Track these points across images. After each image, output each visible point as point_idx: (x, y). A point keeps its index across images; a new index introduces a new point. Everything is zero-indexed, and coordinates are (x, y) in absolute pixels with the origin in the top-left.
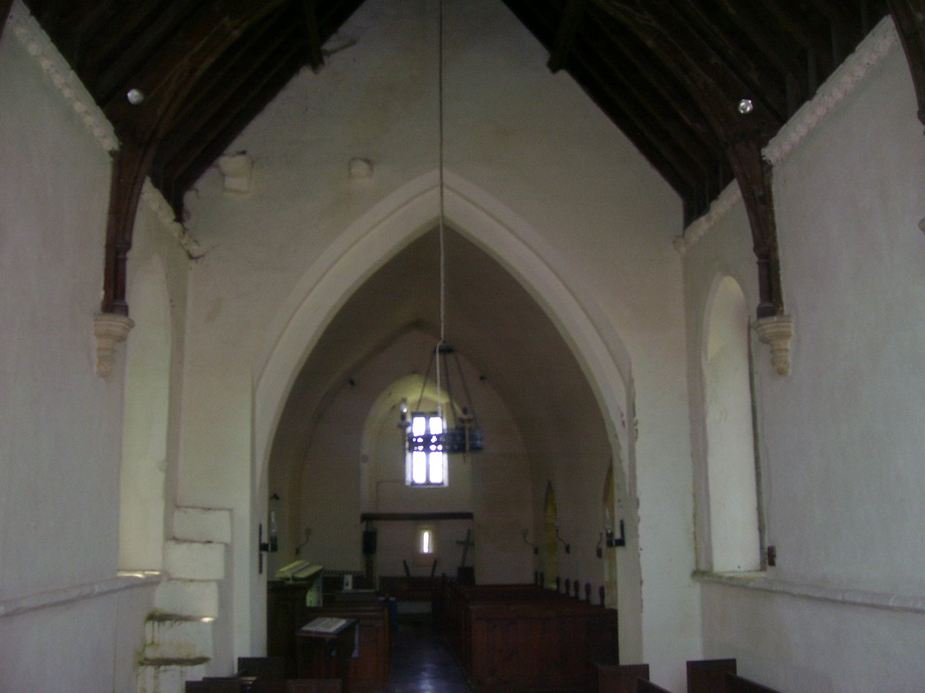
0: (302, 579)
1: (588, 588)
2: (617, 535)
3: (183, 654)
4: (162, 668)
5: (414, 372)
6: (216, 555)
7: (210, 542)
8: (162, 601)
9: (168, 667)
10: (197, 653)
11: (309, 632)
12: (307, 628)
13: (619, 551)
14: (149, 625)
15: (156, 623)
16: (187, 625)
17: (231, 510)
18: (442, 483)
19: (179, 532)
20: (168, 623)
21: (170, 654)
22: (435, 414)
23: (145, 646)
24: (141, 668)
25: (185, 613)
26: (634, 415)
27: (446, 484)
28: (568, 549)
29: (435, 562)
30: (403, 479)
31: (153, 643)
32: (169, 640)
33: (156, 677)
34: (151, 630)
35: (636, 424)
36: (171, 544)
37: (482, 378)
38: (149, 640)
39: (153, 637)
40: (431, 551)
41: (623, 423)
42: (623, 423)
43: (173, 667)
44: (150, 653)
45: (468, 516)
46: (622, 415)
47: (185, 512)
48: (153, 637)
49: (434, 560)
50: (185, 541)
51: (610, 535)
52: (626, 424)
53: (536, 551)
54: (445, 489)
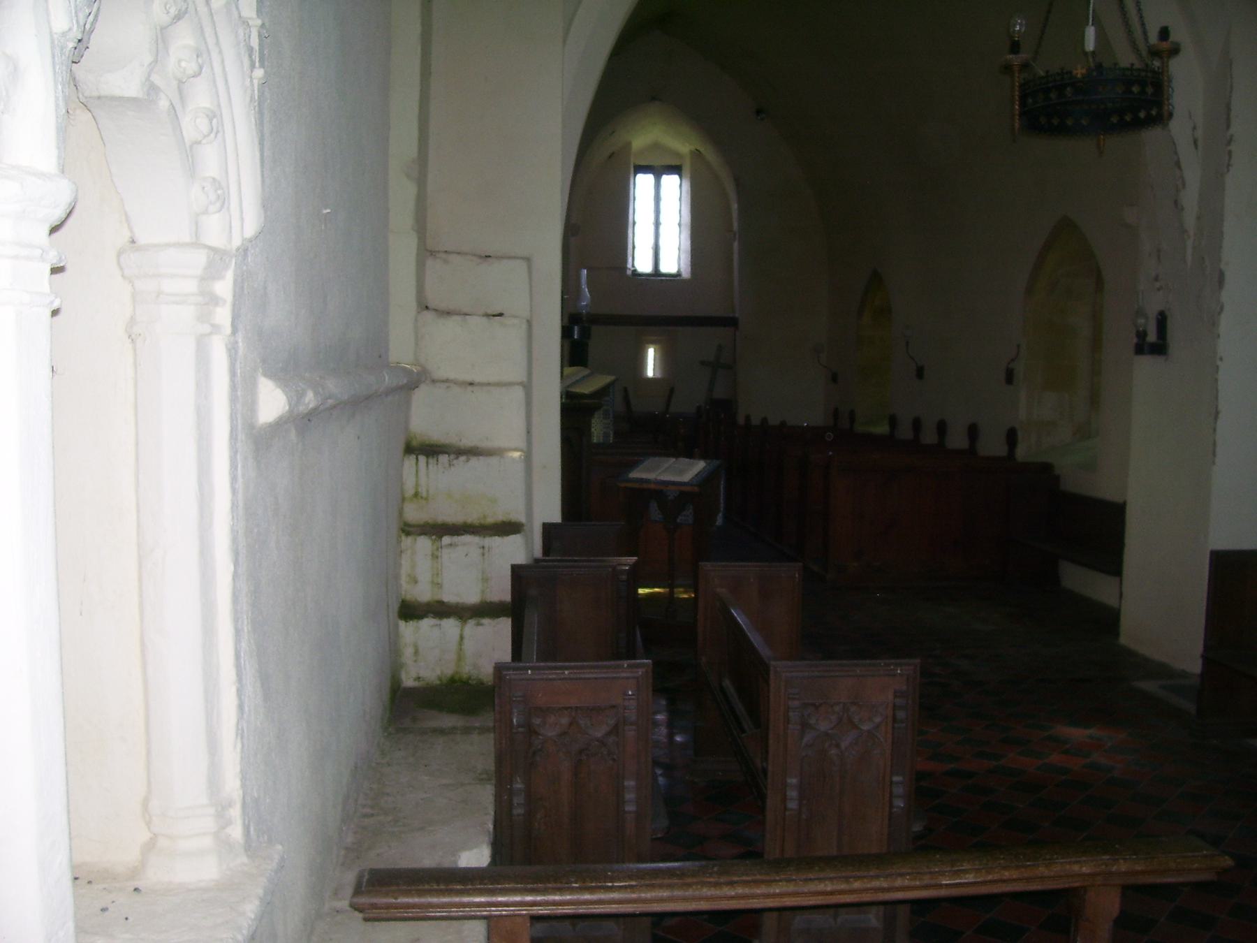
0: (583, 396)
1: (917, 425)
2: (1152, 337)
3: (473, 517)
4: (446, 540)
5: (653, 99)
6: (510, 337)
7: (501, 315)
8: (426, 418)
9: (456, 539)
10: (498, 514)
11: (642, 481)
12: (635, 474)
13: (1146, 366)
14: (410, 462)
15: (422, 459)
16: (494, 460)
17: (528, 260)
18: (678, 274)
19: (433, 299)
20: (444, 459)
21: (449, 514)
22: (675, 169)
23: (403, 499)
24: (407, 541)
25: (467, 442)
26: (1228, 127)
27: (686, 274)
28: (920, 373)
29: (672, 391)
30: (625, 268)
31: (416, 495)
32: (447, 488)
33: (435, 557)
34: (414, 472)
35: (1229, 142)
36: (429, 316)
37: (758, 112)
38: (410, 492)
39: (417, 485)
40: (658, 375)
41: (1195, 142)
42: (1195, 142)
43: (467, 538)
44: (414, 514)
45: (729, 322)
46: (1194, 128)
47: (446, 261)
48: (417, 485)
49: (667, 385)
50: (448, 313)
51: (1142, 335)
52: (1200, 144)
53: (834, 378)
54: (685, 281)
